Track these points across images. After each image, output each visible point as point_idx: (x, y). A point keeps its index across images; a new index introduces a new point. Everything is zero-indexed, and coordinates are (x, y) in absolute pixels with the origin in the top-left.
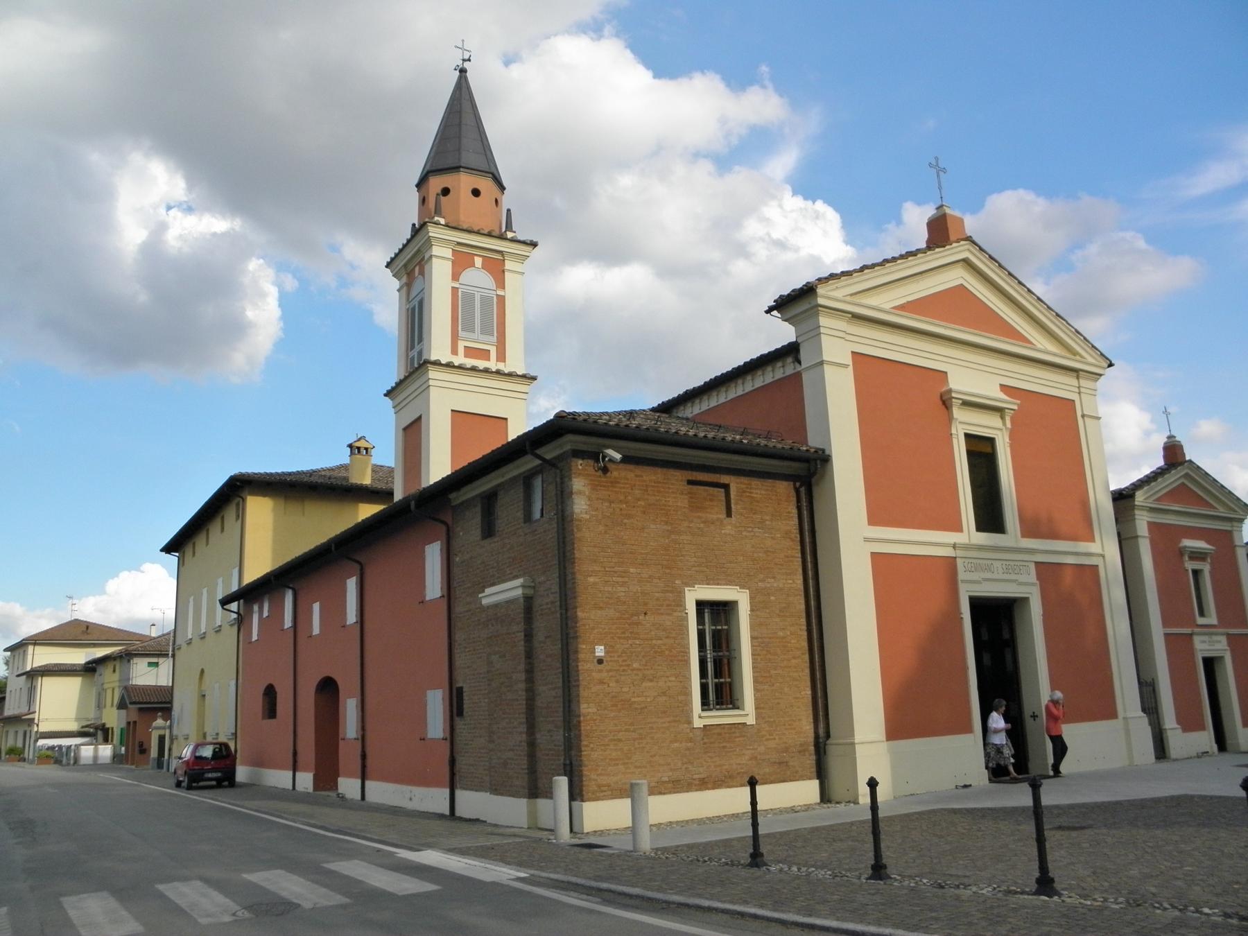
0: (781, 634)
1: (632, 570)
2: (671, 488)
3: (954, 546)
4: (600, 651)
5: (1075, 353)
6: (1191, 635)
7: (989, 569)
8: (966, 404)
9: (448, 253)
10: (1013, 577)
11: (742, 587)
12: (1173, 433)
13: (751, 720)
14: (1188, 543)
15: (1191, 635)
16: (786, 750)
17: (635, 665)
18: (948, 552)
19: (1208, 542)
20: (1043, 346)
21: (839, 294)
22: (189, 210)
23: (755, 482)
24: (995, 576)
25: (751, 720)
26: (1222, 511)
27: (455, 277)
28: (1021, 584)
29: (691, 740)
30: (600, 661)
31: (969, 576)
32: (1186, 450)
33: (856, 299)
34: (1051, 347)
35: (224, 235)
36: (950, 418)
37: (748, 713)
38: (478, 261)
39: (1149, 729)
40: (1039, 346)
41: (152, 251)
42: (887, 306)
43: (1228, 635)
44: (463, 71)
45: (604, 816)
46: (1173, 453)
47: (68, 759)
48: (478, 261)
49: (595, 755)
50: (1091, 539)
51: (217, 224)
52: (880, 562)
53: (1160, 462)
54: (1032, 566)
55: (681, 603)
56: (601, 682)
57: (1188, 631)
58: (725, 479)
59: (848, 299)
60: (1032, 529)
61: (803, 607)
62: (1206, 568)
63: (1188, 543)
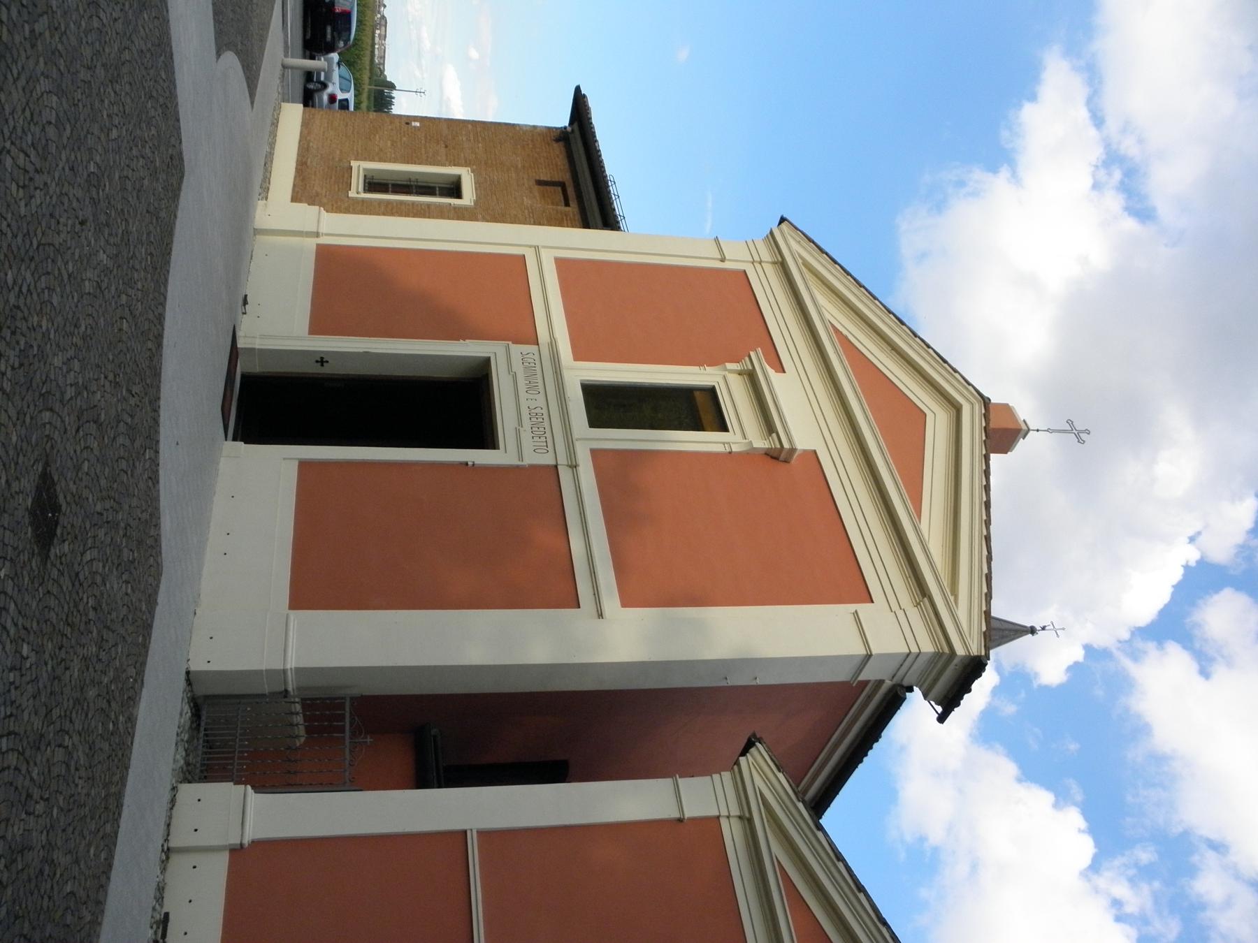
7: (531, 387)
13: (352, 194)
20: (929, 531)
24: (523, 395)
28: (518, 433)
33: (808, 275)
34: (822, 300)
40: (924, 526)
60: (616, 474)
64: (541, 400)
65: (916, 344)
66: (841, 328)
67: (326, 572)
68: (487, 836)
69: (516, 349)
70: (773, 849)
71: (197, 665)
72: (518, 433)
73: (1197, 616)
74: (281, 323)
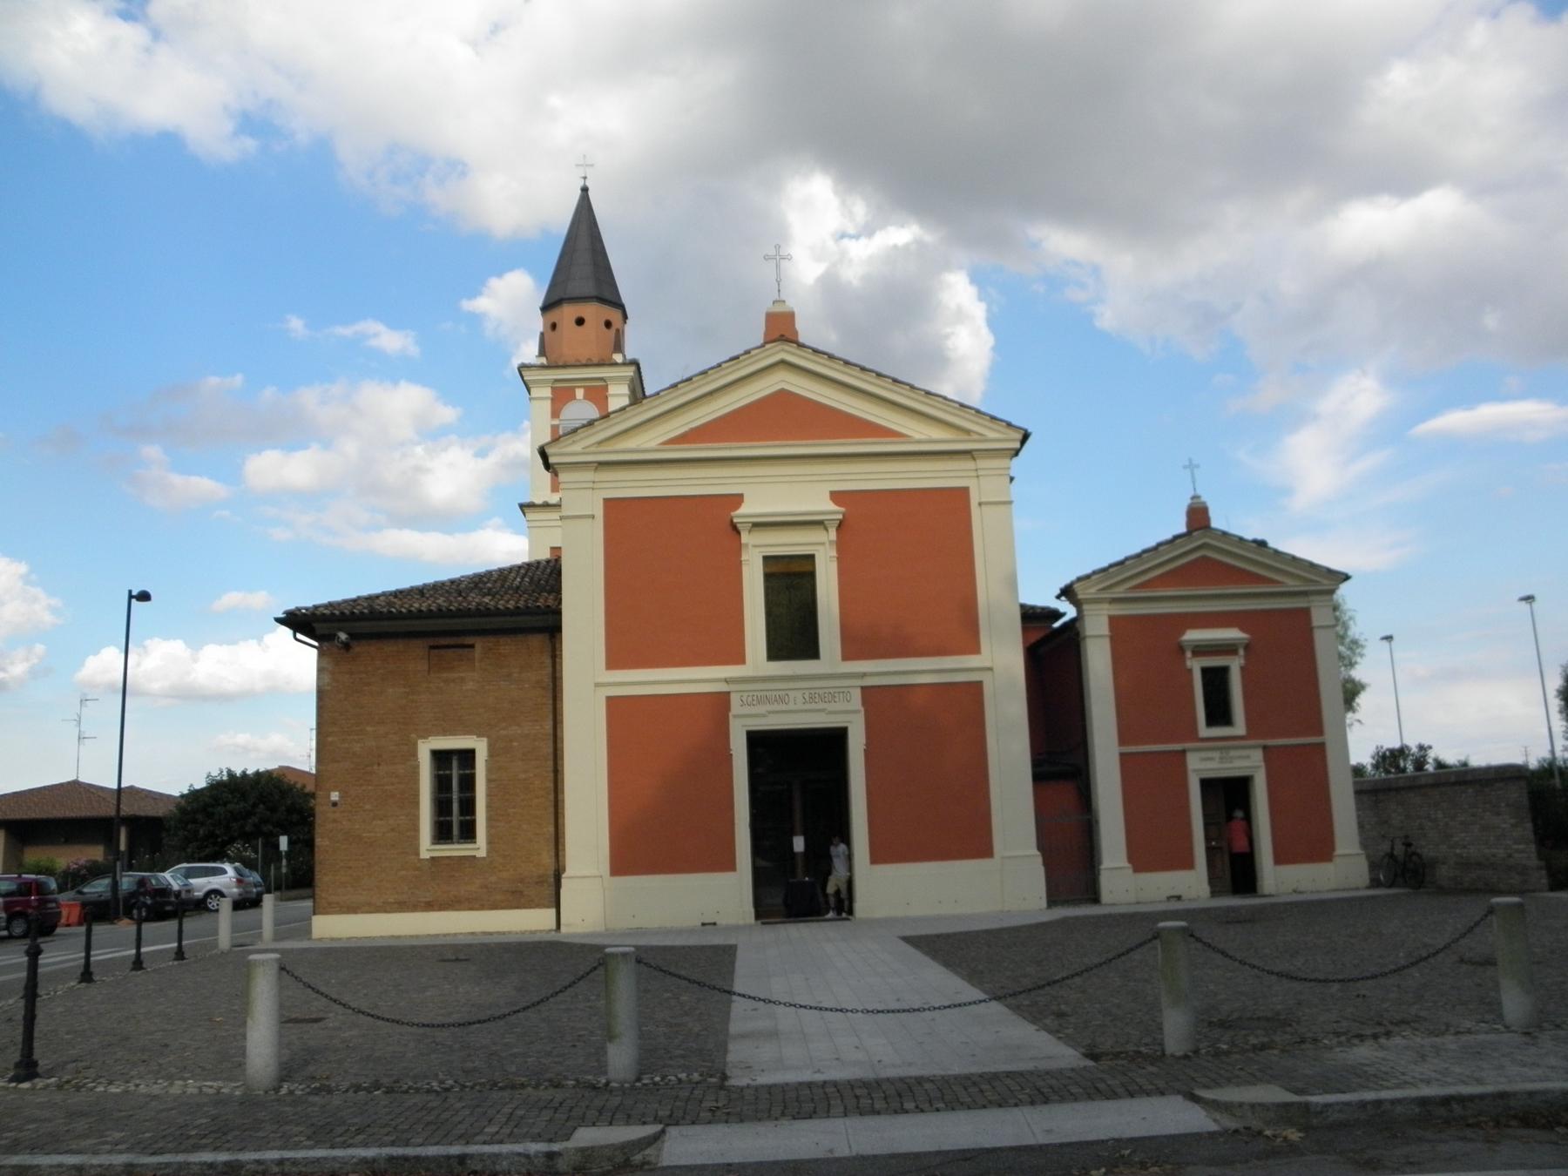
0: (523, 776)
1: (369, 729)
2: (414, 657)
3: (726, 681)
4: (335, 796)
5: (968, 432)
6: (1184, 752)
7: (782, 700)
8: (756, 525)
9: (547, 392)
10: (821, 706)
11: (479, 736)
12: (1199, 492)
13: (482, 853)
14: (1193, 635)
15: (1184, 752)
16: (522, 881)
17: (368, 807)
18: (723, 688)
19: (1242, 629)
20: (920, 433)
21: (577, 448)
22: (868, 231)
23: (503, 640)
24: (791, 706)
25: (482, 853)
26: (1292, 585)
27: (555, 413)
28: (831, 713)
29: (418, 869)
30: (335, 804)
31: (747, 710)
32: (1212, 514)
33: (602, 448)
34: (936, 433)
35: (907, 246)
36: (739, 548)
37: (480, 847)
38: (580, 393)
39: (1042, 870)
40: (917, 436)
41: (830, 285)
42: (653, 444)
43: (1265, 748)
44: (585, 190)
45: (331, 927)
46: (1198, 516)
47: (95, 871)
48: (580, 393)
49: (326, 879)
50: (975, 649)
51: (902, 235)
52: (619, 709)
53: (1181, 528)
54: (858, 691)
55: (414, 754)
56: (335, 821)
57: (1178, 747)
58: (469, 640)
59: (593, 449)
60: (855, 646)
61: (551, 750)
62: (1235, 665)
63: (1193, 635)
64: (799, 694)
65: (713, 375)
66: (672, 435)
67: (969, 837)
68: (1123, 740)
69: (736, 707)
70: (1119, 592)
71: (1044, 903)
72: (831, 713)
73: (856, 283)
74: (1191, 884)
